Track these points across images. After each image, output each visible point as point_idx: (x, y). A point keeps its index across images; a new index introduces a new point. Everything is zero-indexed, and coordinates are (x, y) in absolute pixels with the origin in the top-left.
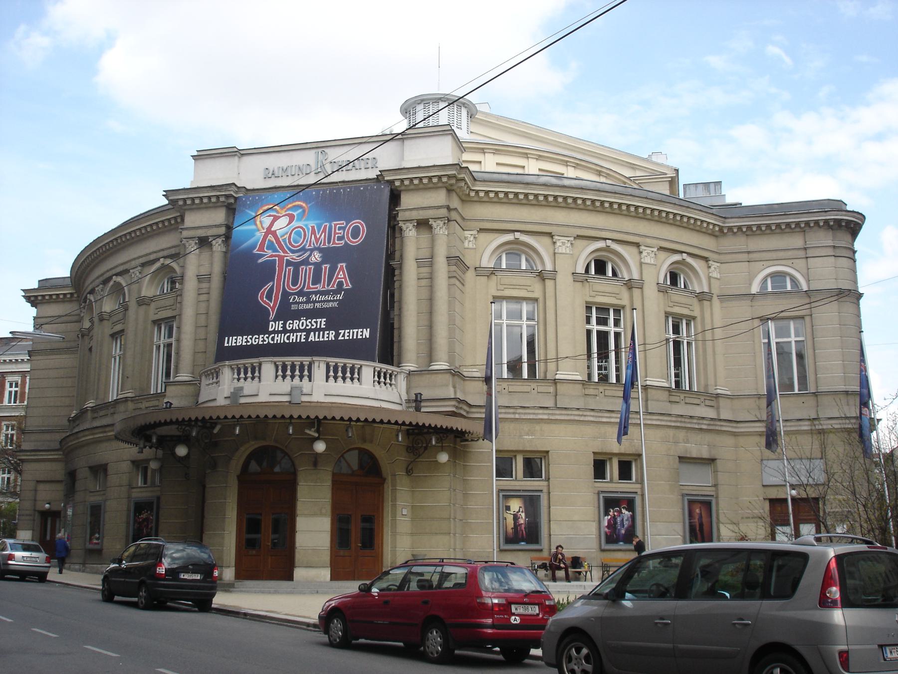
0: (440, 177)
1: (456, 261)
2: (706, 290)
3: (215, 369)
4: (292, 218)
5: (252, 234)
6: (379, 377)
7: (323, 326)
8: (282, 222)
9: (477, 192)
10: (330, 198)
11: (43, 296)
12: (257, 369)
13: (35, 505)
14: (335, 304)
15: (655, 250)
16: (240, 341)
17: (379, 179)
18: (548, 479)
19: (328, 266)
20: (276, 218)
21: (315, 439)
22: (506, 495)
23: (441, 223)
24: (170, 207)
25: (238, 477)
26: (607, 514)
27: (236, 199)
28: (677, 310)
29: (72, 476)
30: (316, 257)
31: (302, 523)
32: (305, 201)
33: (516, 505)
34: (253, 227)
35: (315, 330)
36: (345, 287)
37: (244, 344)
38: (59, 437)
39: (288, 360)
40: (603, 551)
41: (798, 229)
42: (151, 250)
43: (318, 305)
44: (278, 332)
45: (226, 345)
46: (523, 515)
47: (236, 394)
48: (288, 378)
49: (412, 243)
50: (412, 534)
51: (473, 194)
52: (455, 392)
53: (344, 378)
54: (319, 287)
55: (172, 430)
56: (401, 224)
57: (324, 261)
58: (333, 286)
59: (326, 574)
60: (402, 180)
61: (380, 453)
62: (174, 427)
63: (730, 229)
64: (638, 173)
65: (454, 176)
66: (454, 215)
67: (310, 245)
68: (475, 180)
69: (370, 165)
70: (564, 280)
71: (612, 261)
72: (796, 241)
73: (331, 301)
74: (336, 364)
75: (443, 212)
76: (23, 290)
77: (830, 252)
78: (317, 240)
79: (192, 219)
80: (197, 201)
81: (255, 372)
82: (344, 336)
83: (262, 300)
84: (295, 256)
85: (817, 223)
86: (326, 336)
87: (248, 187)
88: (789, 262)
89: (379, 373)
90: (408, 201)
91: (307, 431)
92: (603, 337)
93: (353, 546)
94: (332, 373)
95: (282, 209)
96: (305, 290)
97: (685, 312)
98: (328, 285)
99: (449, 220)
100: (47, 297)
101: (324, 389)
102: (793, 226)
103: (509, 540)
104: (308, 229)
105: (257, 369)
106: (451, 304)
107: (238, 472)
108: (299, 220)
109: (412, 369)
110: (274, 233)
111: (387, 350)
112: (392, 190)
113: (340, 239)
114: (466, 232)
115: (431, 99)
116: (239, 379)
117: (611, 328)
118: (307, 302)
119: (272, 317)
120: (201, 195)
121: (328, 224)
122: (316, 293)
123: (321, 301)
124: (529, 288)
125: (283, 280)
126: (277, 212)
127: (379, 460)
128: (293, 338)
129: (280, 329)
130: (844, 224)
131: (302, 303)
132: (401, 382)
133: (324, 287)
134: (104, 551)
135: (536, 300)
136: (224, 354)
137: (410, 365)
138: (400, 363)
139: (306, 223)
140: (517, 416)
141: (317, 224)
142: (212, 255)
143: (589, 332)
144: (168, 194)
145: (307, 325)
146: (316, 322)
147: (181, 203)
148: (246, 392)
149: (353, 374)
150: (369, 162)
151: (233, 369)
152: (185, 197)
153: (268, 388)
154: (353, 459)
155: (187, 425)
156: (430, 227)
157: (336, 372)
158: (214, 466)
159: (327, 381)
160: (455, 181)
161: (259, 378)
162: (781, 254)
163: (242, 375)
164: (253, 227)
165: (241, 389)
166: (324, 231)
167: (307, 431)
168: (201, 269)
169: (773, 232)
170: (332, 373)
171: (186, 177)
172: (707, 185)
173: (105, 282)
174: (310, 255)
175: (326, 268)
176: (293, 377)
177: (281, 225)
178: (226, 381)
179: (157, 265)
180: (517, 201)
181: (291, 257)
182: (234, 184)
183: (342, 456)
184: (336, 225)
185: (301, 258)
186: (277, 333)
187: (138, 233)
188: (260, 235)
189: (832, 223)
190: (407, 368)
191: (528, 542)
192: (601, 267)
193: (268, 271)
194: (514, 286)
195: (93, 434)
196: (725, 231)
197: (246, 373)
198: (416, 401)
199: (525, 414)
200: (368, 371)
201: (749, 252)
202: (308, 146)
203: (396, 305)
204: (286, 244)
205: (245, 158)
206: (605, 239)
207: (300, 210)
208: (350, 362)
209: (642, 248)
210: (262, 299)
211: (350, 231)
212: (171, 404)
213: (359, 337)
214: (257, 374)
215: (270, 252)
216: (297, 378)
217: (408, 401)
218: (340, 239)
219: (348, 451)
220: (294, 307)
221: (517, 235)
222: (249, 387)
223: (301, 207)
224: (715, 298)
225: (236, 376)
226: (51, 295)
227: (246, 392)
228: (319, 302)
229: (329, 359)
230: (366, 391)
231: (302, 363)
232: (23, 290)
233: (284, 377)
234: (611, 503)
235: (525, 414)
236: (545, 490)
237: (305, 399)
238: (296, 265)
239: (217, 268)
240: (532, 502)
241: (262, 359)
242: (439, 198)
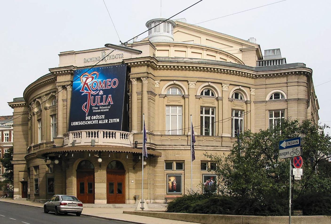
0: (144, 62)
1: (151, 93)
2: (249, 99)
5: (79, 84)
7: (104, 118)
8: (90, 79)
9: (159, 66)
10: (106, 71)
11: (15, 105)
12: (80, 134)
13: (19, 179)
14: (108, 110)
15: (228, 85)
16: (76, 123)
17: (123, 62)
18: (184, 170)
19: (105, 96)
20: (87, 78)
21: (98, 158)
22: (169, 176)
23: (145, 79)
24: (51, 74)
25: (76, 170)
27: (74, 71)
28: (237, 108)
29: (29, 169)
30: (101, 93)
31: (96, 185)
32: (97, 71)
33: (173, 179)
34: (80, 82)
35: (101, 119)
36: (111, 104)
37: (78, 125)
38: (25, 155)
39: (90, 131)
40: (167, 194)
41: (285, 75)
43: (102, 110)
44: (89, 120)
45: (72, 125)
46: (175, 182)
47: (73, 143)
48: (91, 137)
49: (135, 86)
50: (136, 189)
51: (158, 67)
52: (150, 141)
53: (110, 137)
54: (102, 104)
55: (53, 155)
56: (131, 79)
57: (104, 95)
58: (107, 103)
59: (105, 201)
60: (131, 63)
61: (123, 162)
62: (54, 154)
63: (259, 75)
64: (244, 47)
65: (149, 61)
66: (150, 76)
67: (99, 88)
69: (121, 57)
70: (192, 98)
71: (211, 90)
72: (284, 80)
73: (106, 109)
74: (110, 132)
75: (146, 75)
76: (8, 103)
77: (296, 84)
78: (101, 86)
79: (60, 79)
81: (80, 135)
82: (111, 121)
83: (83, 109)
84: (94, 92)
85: (292, 72)
86: (105, 121)
87: (78, 67)
88: (280, 88)
89: (122, 134)
90: (134, 70)
91: (95, 155)
92: (207, 118)
93: (115, 192)
94: (105, 135)
95: (89, 75)
96: (98, 105)
98: (105, 103)
99: (148, 78)
100: (17, 105)
101: (102, 141)
102: (283, 74)
103: (170, 191)
104: (98, 82)
105: (80, 134)
106: (149, 109)
107: (76, 169)
109: (135, 132)
110: (87, 84)
111: (126, 126)
114: (156, 81)
115: (157, 21)
116: (75, 138)
117: (210, 116)
119: (87, 115)
120: (62, 70)
121: (105, 80)
122: (101, 106)
123: (103, 109)
124: (179, 102)
125: (90, 102)
126: (88, 76)
127: (124, 165)
128: (94, 122)
129: (90, 119)
130: (302, 73)
131: (97, 109)
132: (131, 137)
133: (104, 104)
134: (40, 195)
135: (182, 106)
136: (71, 128)
137: (135, 131)
138: (131, 130)
139: (98, 80)
140: (173, 148)
141: (101, 80)
143: (202, 117)
144: (50, 70)
145: (98, 118)
146: (101, 117)
147: (55, 73)
148: (77, 142)
149: (113, 135)
150: (121, 55)
152: (56, 71)
153: (84, 140)
154: (114, 164)
156: (141, 81)
157: (107, 134)
158: (68, 166)
159: (104, 138)
160: (151, 63)
161: (81, 137)
163: (76, 136)
164: (80, 82)
165: (76, 141)
166: (104, 83)
167: (95, 155)
168: (64, 97)
169: (275, 77)
170: (105, 135)
171: (56, 63)
172: (274, 50)
173: (34, 101)
174: (99, 92)
175: (104, 96)
176: (92, 137)
177: (89, 81)
179: (50, 95)
180: (175, 68)
181: (93, 93)
182: (72, 66)
183: (110, 163)
184: (108, 81)
185: (96, 94)
186: (89, 120)
188: (82, 85)
189: (297, 73)
190: (133, 132)
191: (177, 191)
192: (237, 97)
193: (85, 98)
194: (174, 101)
195: (34, 155)
197: (77, 135)
198: (135, 144)
199: (176, 147)
200: (118, 133)
201: (266, 85)
202: (99, 50)
203: (130, 109)
204: (91, 88)
205: (77, 55)
206: (208, 82)
207: (96, 75)
208: (111, 131)
209: (223, 85)
210: (83, 108)
211: (112, 83)
212: (55, 146)
213: (116, 122)
214: (80, 136)
215: (85, 91)
216: (93, 137)
217: (133, 144)
218: (109, 86)
219: (112, 161)
220: (94, 111)
221: (175, 82)
222: (78, 140)
223: (95, 74)
224: (252, 102)
225: (74, 136)
226: (18, 104)
227: (77, 142)
228: (102, 109)
229: (104, 130)
230: (118, 141)
231: (95, 132)
232: (8, 103)
233: (89, 137)
234: (207, 178)
235: (176, 147)
236: (183, 174)
237: (96, 144)
238: (95, 96)
239: (69, 97)
240: (178, 178)
241: (82, 131)
242: (144, 69)
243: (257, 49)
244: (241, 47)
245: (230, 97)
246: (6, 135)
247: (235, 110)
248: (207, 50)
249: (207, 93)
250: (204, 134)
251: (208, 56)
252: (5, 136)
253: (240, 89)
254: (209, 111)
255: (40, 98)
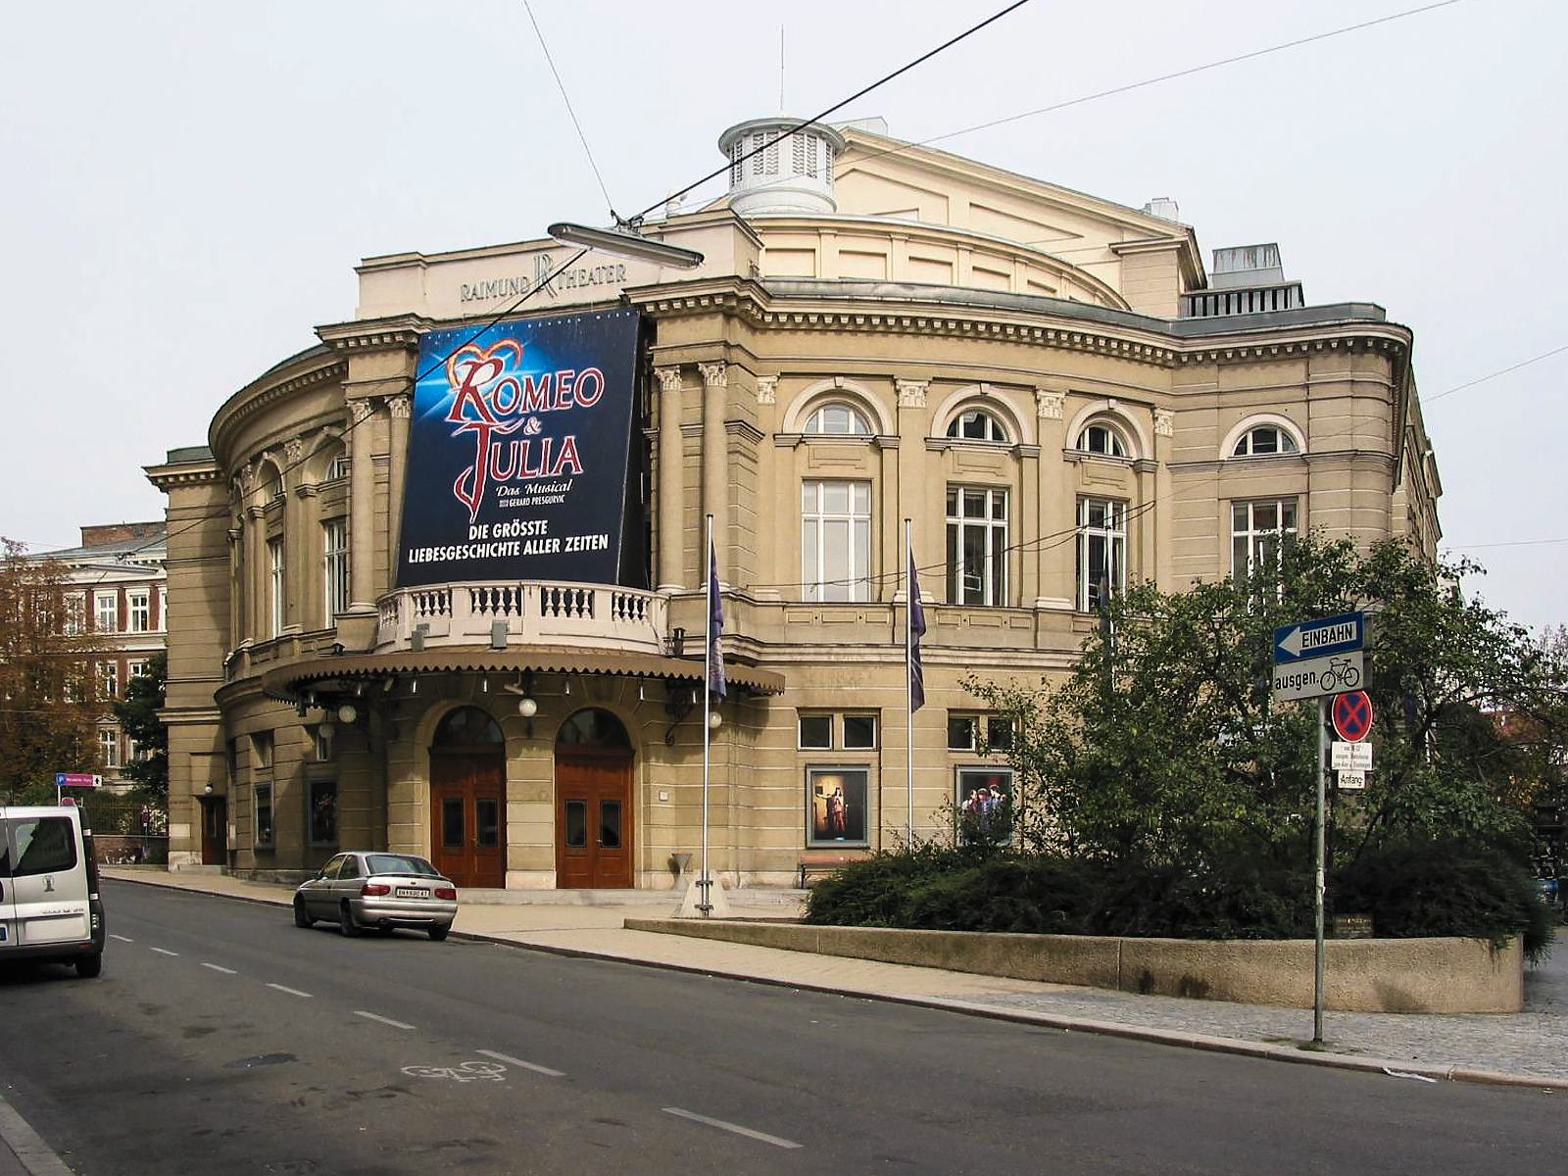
0: (711, 297)
1: (741, 428)
2: (1148, 455)
3: (392, 598)
4: (498, 366)
5: (442, 392)
6: (622, 606)
7: (543, 532)
9: (776, 315)
10: (552, 337)
11: (176, 477)
12: (447, 598)
14: (561, 499)
15: (1062, 396)
16: (429, 555)
17: (623, 300)
18: (879, 749)
19: (550, 440)
20: (476, 367)
22: (818, 772)
23: (716, 369)
24: (325, 349)
26: (966, 796)
28: (1098, 489)
29: (231, 743)
30: (534, 427)
33: (830, 785)
34: (445, 381)
35: (532, 538)
36: (574, 472)
37: (436, 559)
38: (215, 687)
39: (488, 585)
40: (809, 849)
42: (311, 415)
43: (536, 500)
44: (481, 542)
45: (411, 561)
46: (841, 799)
47: (417, 637)
48: (489, 610)
50: (677, 826)
51: (768, 319)
52: (737, 629)
53: (568, 611)
54: (538, 473)
55: (333, 686)
56: (657, 371)
57: (543, 435)
58: (557, 471)
59: (551, 879)
60: (656, 303)
61: (626, 716)
63: (1192, 355)
64: (1128, 237)
65: (732, 295)
66: (737, 355)
67: (524, 409)
68: (771, 297)
69: (614, 277)
71: (993, 415)
72: (1295, 373)
73: (554, 494)
75: (718, 351)
77: (1345, 390)
78: (534, 400)
79: (361, 370)
80: (363, 342)
82: (572, 545)
84: (503, 425)
85: (1327, 343)
86: (548, 546)
87: (436, 318)
88: (1280, 409)
89: (621, 600)
90: (668, 334)
91: (507, 687)
92: (975, 534)
94: (550, 603)
95: (484, 353)
96: (519, 477)
97: (1113, 492)
98: (550, 472)
99: (728, 364)
100: (182, 479)
101: (539, 627)
102: (1290, 350)
103: (819, 835)
105: (447, 598)
106: (732, 495)
107: (429, 743)
108: (509, 369)
110: (474, 391)
111: (636, 565)
112: (635, 324)
113: (567, 397)
114: (760, 379)
116: (423, 613)
117: (989, 522)
118: (521, 496)
119: (473, 519)
120: (368, 333)
121: (550, 375)
122: (533, 482)
123: (542, 495)
126: (477, 356)
127: (627, 726)
128: (502, 549)
129: (485, 537)
130: (1370, 344)
131: (514, 497)
132: (657, 613)
133: (544, 473)
134: (277, 851)
135: (869, 481)
136: (408, 575)
137: (672, 587)
138: (658, 583)
139: (519, 373)
140: (833, 658)
141: (535, 376)
142: (390, 423)
143: (952, 530)
145: (521, 531)
146: (534, 526)
147: (340, 345)
148: (432, 631)
149: (583, 604)
150: (614, 271)
151: (415, 599)
152: (346, 335)
153: (461, 624)
154: (586, 723)
155: (353, 680)
157: (556, 601)
159: (543, 614)
160: (740, 304)
161: (450, 611)
162: (1271, 396)
163: (427, 607)
164: (445, 381)
165: (427, 627)
166: (545, 385)
167: (507, 687)
168: (378, 446)
169: (1258, 361)
170: (550, 603)
172: (1251, 250)
174: (525, 424)
175: (547, 442)
176: (495, 609)
177: (483, 377)
178: (407, 616)
179: (321, 437)
180: (838, 326)
181: (498, 426)
182: (414, 315)
183: (569, 719)
184: (561, 376)
185: (510, 430)
186: (483, 542)
187: (305, 382)
188: (453, 394)
190: (668, 591)
191: (847, 838)
192: (1097, 444)
194: (835, 461)
195: (252, 688)
196: (1185, 359)
197: (432, 604)
198: (675, 639)
200: (603, 596)
202: (525, 248)
203: (653, 495)
204: (490, 407)
205: (432, 269)
206: (980, 382)
207: (511, 354)
208: (575, 586)
209: (1040, 393)
210: (459, 492)
211: (580, 387)
212: (342, 647)
213: (594, 547)
214: (447, 606)
215: (468, 421)
216: (501, 610)
217: (667, 640)
218: (567, 397)
220: (502, 504)
221: (840, 380)
222: (436, 623)
223: (509, 348)
224: (1162, 468)
225: (419, 608)
226: (187, 475)
227: (432, 631)
228: (537, 495)
229: (544, 583)
230: (604, 629)
231: (507, 588)
233: (483, 609)
234: (974, 782)
236: (875, 763)
237: (511, 640)
238: (506, 440)
240: (855, 783)
241: (451, 585)
242: (711, 329)
243: (1184, 244)
244: (1114, 238)
245: (1072, 445)
246: (103, 605)
247: (1091, 497)
248: (975, 249)
249: (975, 430)
250: (961, 600)
251: (978, 274)
252: (131, 608)
253: (1110, 413)
254: (981, 502)
255: (277, 448)
